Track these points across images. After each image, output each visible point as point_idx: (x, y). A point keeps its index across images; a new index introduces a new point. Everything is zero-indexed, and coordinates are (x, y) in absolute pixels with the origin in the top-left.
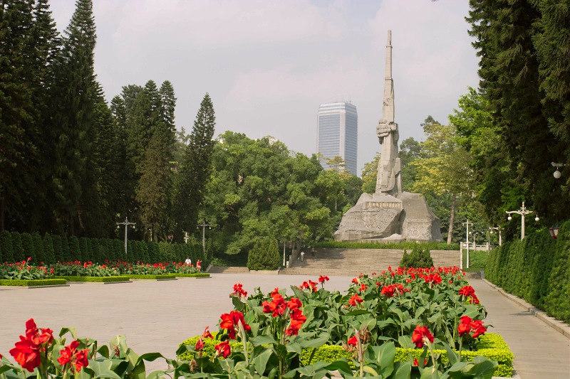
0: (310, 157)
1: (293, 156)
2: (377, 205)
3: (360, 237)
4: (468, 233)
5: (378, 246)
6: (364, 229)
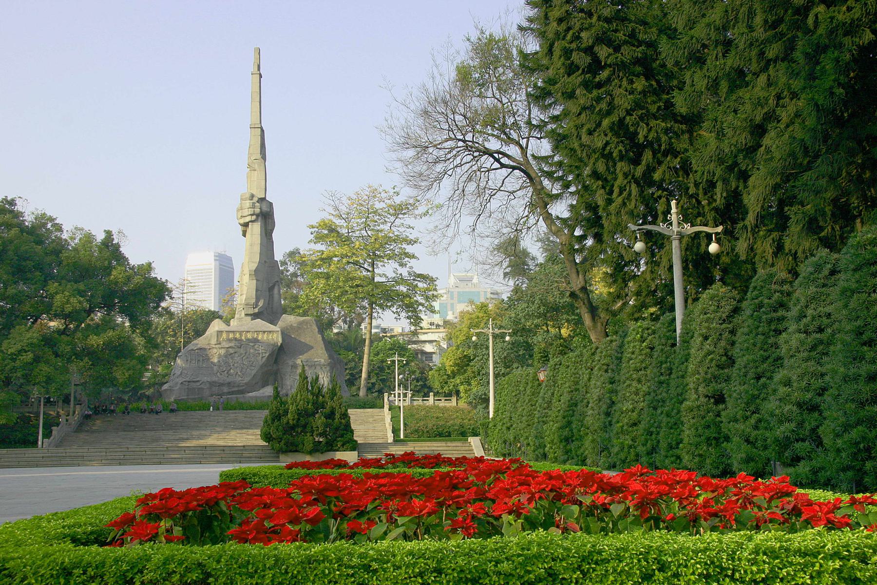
0: (100, 237)
1: (29, 219)
2: (238, 335)
3: (207, 393)
4: (398, 377)
5: (241, 407)
6: (215, 379)
